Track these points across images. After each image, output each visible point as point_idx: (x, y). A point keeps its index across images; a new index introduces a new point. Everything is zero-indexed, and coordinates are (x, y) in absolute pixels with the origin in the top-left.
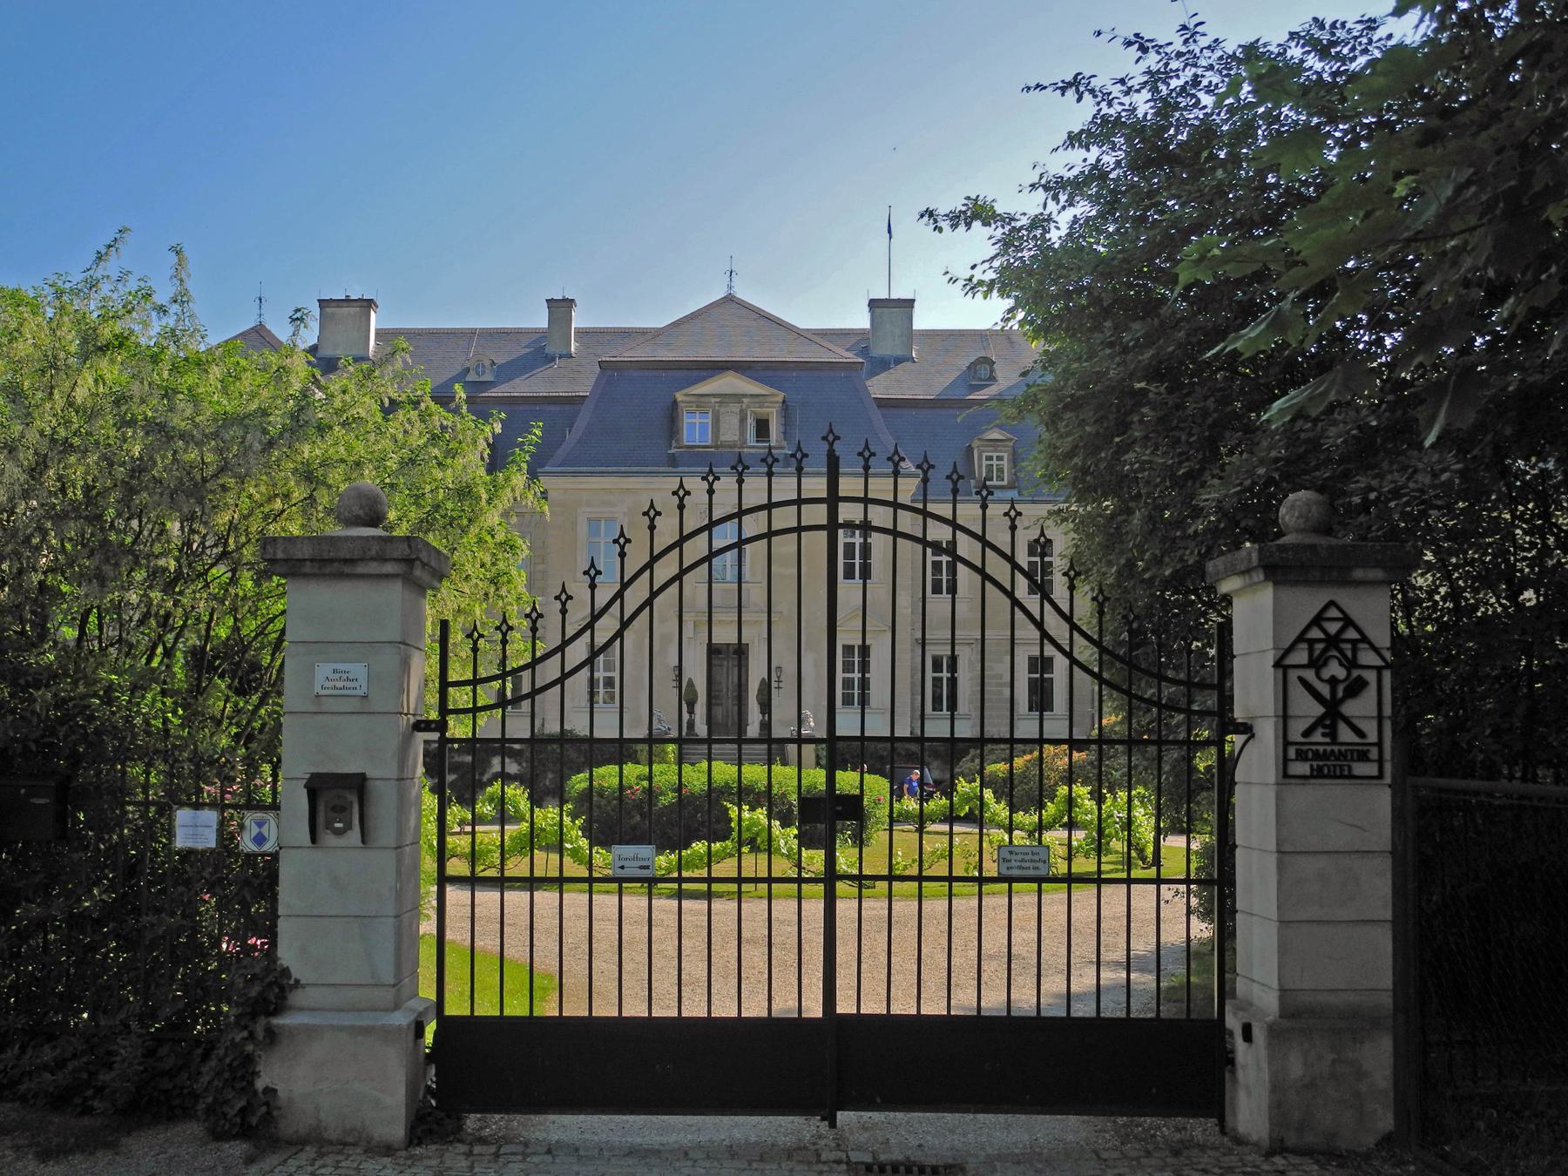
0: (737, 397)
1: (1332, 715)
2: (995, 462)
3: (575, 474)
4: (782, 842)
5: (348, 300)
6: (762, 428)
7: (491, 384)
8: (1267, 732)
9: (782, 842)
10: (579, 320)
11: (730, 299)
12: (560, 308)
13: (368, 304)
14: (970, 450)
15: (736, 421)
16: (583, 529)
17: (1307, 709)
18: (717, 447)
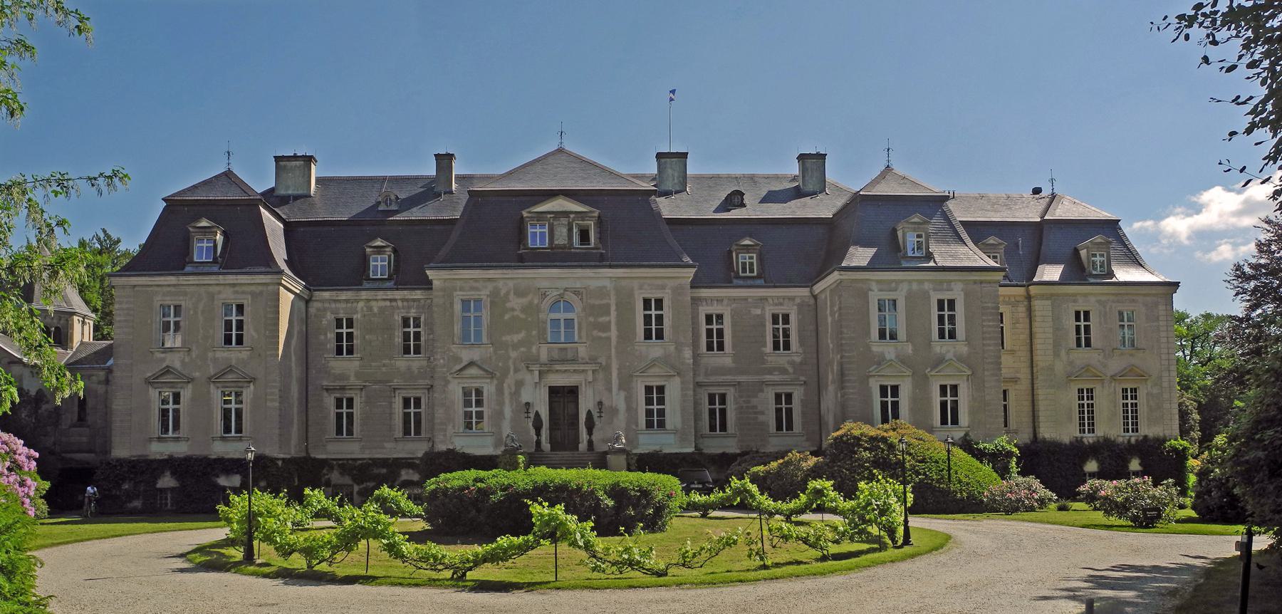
0: (566, 214)
3: (452, 268)
4: (578, 536)
5: (295, 157)
6: (584, 236)
7: (396, 212)
9: (578, 536)
10: (458, 169)
11: (560, 151)
12: (444, 161)
13: (309, 160)
14: (730, 252)
15: (565, 230)
16: (458, 307)
18: (552, 249)
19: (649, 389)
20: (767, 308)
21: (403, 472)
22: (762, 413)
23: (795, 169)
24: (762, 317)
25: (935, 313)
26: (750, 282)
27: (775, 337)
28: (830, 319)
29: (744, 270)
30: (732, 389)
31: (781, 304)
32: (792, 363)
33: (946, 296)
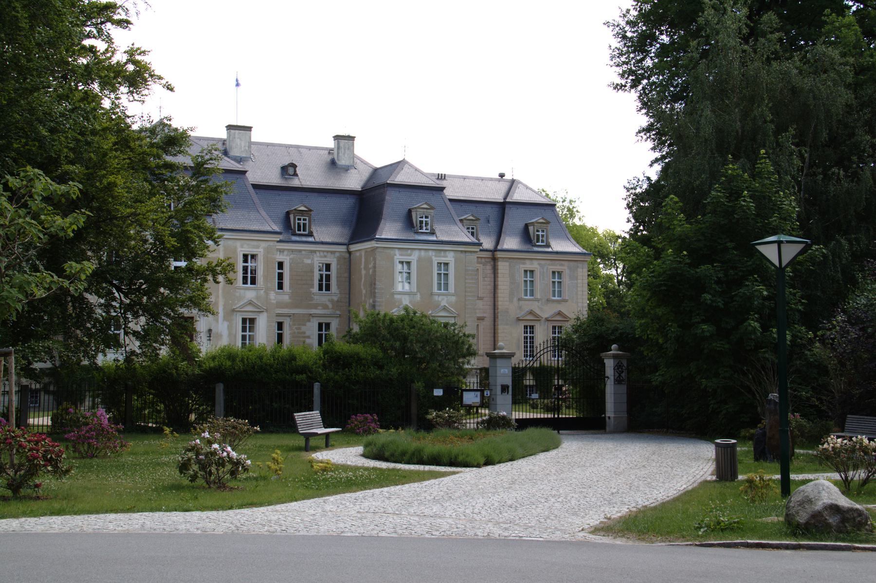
1: (620, 376)
2: (302, 222)
8: (612, 378)
17: (617, 375)
19: (244, 321)
20: (316, 259)
21: (435, 390)
22: (309, 337)
23: (331, 144)
24: (311, 266)
25: (435, 271)
26: (304, 239)
27: (321, 280)
28: (363, 272)
29: (299, 230)
30: (288, 319)
31: (325, 256)
32: (332, 301)
33: (443, 260)
